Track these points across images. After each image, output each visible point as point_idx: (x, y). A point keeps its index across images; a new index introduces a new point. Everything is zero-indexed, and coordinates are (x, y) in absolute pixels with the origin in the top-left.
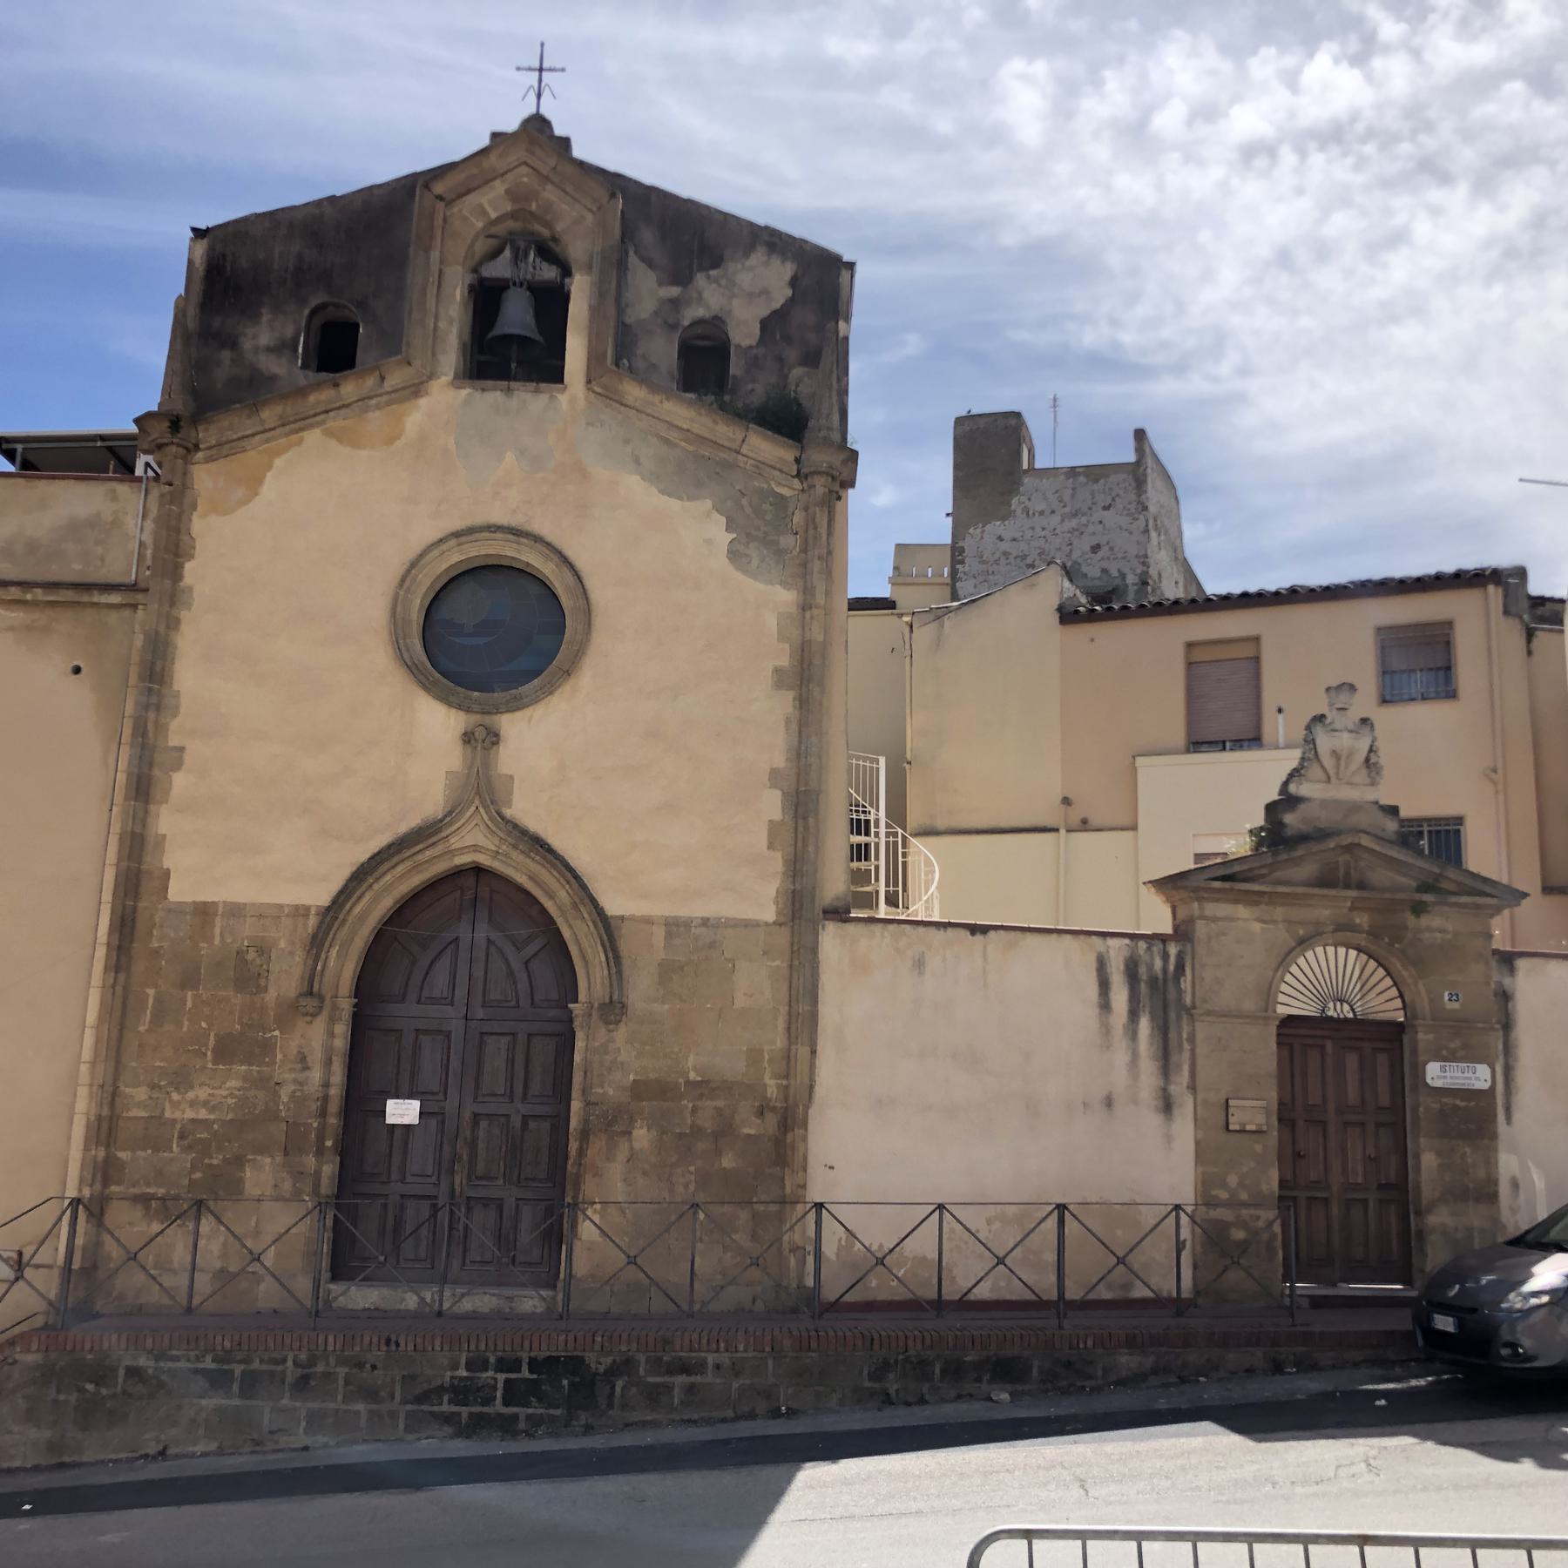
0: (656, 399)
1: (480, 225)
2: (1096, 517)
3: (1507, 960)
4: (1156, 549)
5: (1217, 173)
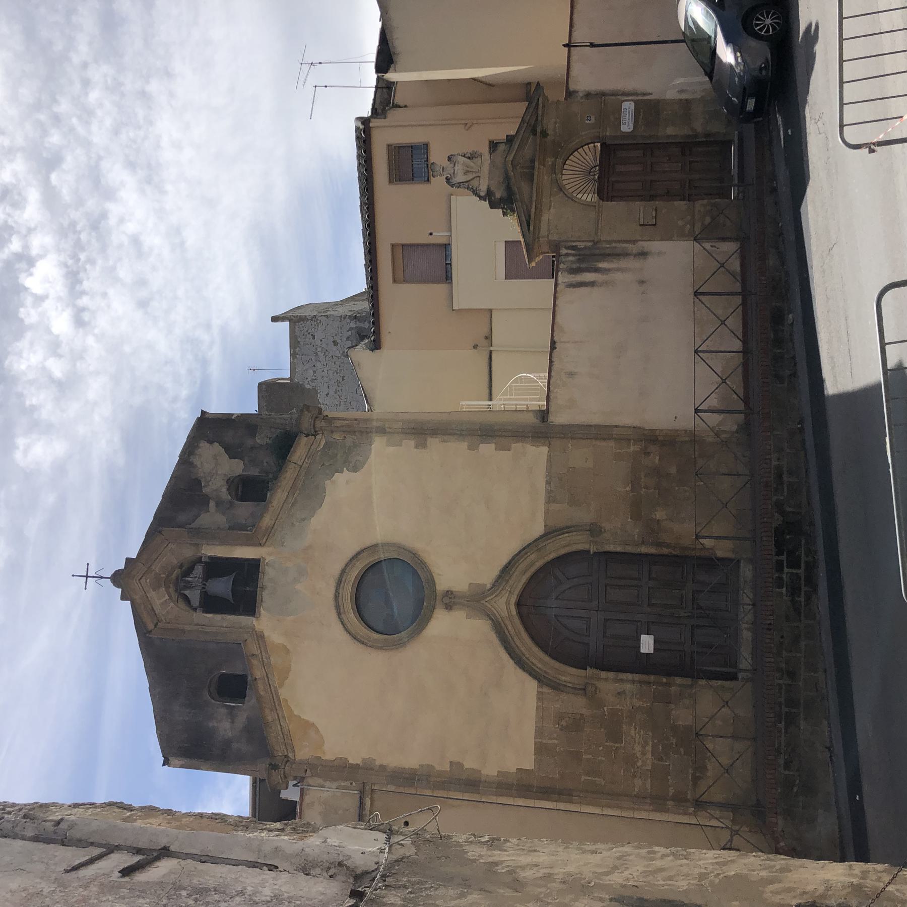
0: (271, 509)
1: (172, 604)
2: (319, 343)
3: (570, 94)
4: (337, 312)
5: (90, 340)
